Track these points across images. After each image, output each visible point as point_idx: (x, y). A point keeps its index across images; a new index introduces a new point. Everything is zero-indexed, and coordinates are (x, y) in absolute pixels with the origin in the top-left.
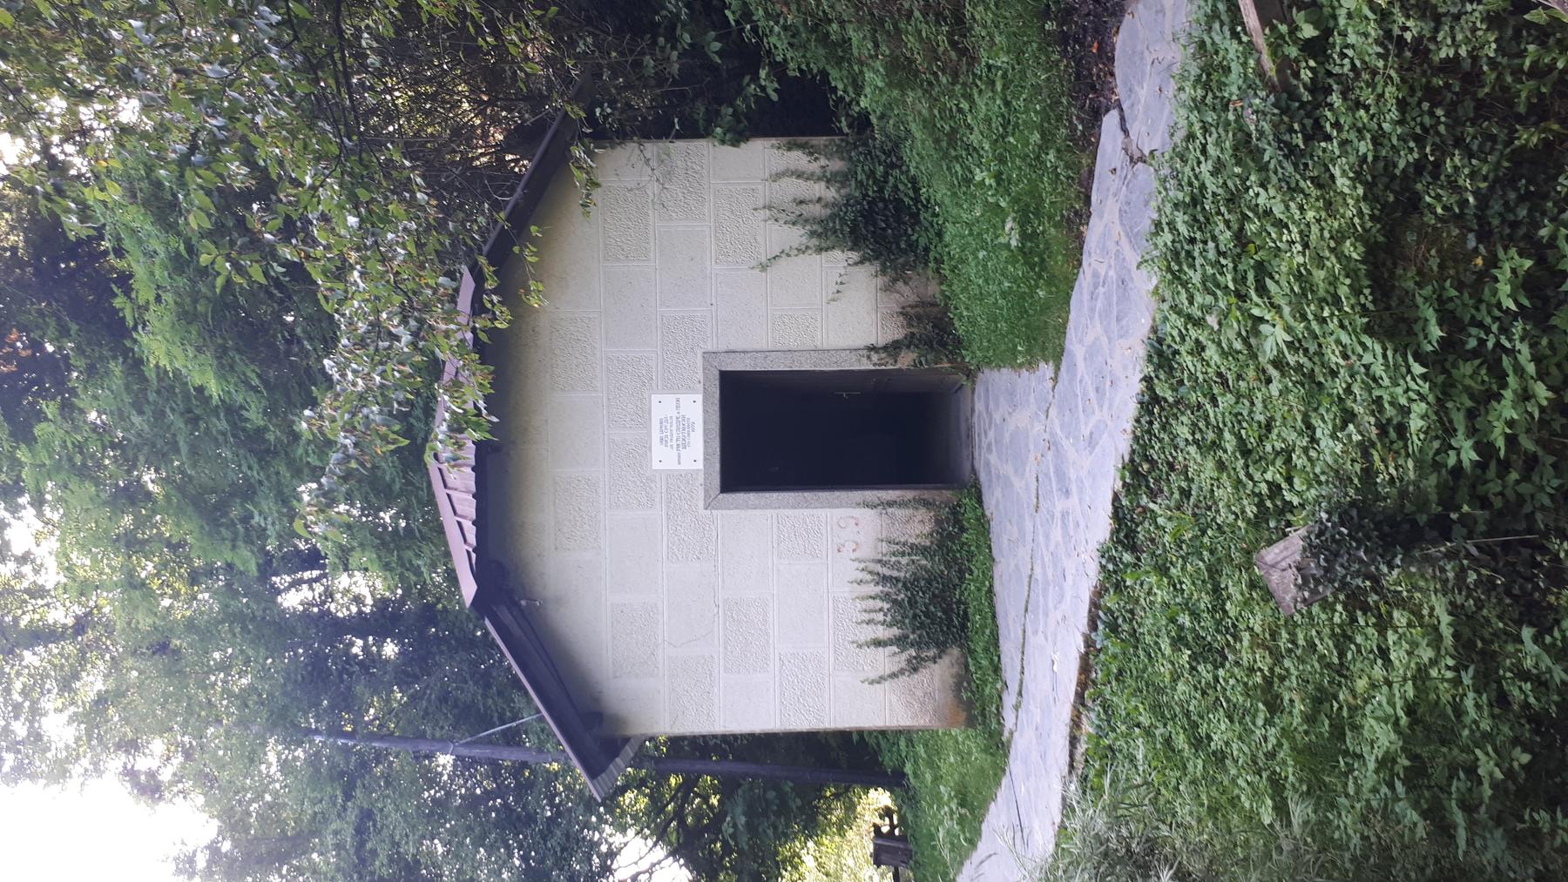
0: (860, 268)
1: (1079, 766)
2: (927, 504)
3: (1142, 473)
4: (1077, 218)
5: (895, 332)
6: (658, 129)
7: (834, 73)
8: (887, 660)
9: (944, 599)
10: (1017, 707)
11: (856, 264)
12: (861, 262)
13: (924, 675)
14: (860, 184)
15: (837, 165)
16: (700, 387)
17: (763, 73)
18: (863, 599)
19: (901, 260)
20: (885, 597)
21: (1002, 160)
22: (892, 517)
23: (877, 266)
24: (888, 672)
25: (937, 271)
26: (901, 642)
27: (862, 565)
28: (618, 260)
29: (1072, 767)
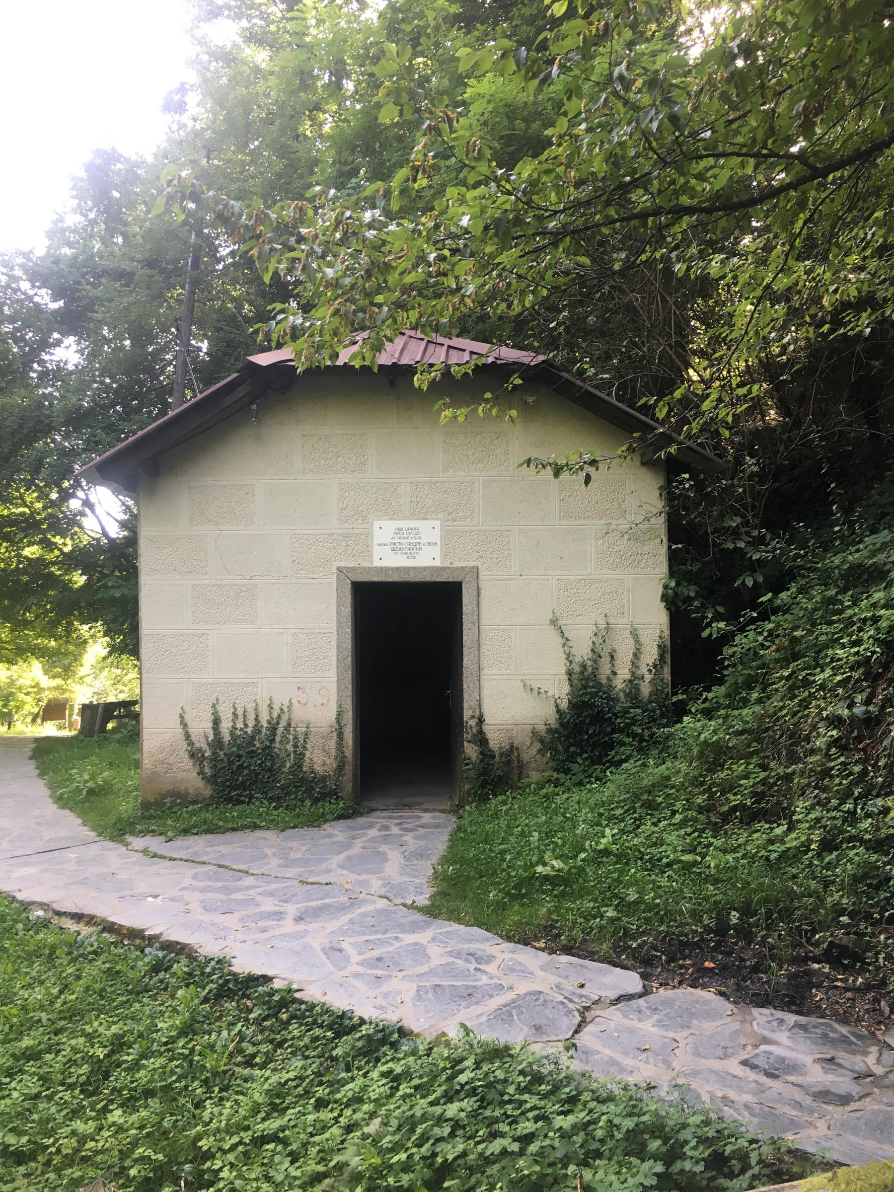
0: (553, 708)
1: (56, 920)
2: (341, 767)
3: (277, 1009)
4: (554, 939)
5: (495, 739)
6: (676, 530)
7: (723, 690)
8: (201, 728)
9: (255, 782)
10: (145, 852)
11: (557, 706)
12: (559, 711)
13: (187, 763)
14: (626, 711)
15: (646, 690)
16: (447, 564)
17: (722, 625)
18: (256, 709)
19: (560, 748)
20: (257, 729)
21: (620, 856)
22: (327, 737)
23: (554, 725)
24: (191, 731)
25: (549, 781)
26: (217, 743)
27: (286, 710)
28: (561, 492)
29: (59, 914)
